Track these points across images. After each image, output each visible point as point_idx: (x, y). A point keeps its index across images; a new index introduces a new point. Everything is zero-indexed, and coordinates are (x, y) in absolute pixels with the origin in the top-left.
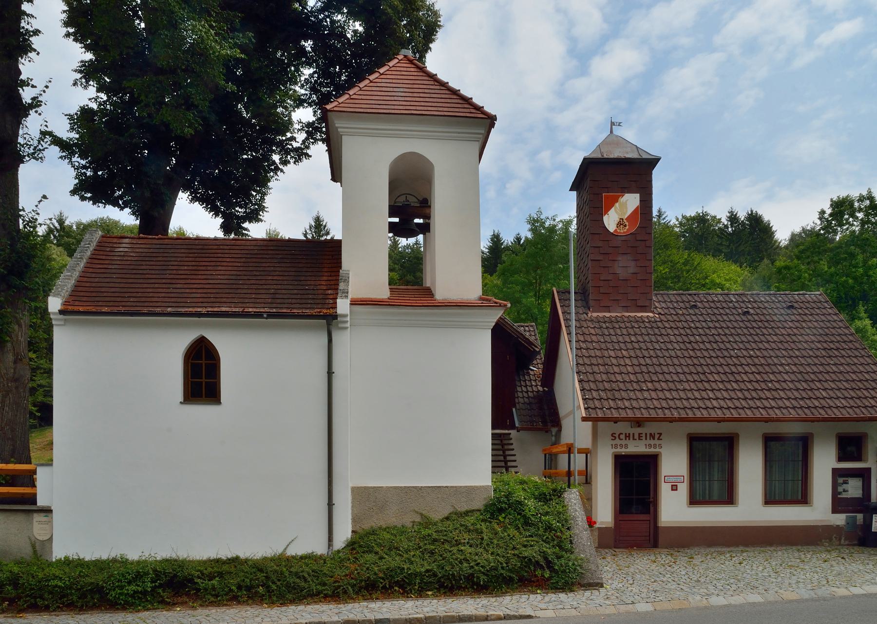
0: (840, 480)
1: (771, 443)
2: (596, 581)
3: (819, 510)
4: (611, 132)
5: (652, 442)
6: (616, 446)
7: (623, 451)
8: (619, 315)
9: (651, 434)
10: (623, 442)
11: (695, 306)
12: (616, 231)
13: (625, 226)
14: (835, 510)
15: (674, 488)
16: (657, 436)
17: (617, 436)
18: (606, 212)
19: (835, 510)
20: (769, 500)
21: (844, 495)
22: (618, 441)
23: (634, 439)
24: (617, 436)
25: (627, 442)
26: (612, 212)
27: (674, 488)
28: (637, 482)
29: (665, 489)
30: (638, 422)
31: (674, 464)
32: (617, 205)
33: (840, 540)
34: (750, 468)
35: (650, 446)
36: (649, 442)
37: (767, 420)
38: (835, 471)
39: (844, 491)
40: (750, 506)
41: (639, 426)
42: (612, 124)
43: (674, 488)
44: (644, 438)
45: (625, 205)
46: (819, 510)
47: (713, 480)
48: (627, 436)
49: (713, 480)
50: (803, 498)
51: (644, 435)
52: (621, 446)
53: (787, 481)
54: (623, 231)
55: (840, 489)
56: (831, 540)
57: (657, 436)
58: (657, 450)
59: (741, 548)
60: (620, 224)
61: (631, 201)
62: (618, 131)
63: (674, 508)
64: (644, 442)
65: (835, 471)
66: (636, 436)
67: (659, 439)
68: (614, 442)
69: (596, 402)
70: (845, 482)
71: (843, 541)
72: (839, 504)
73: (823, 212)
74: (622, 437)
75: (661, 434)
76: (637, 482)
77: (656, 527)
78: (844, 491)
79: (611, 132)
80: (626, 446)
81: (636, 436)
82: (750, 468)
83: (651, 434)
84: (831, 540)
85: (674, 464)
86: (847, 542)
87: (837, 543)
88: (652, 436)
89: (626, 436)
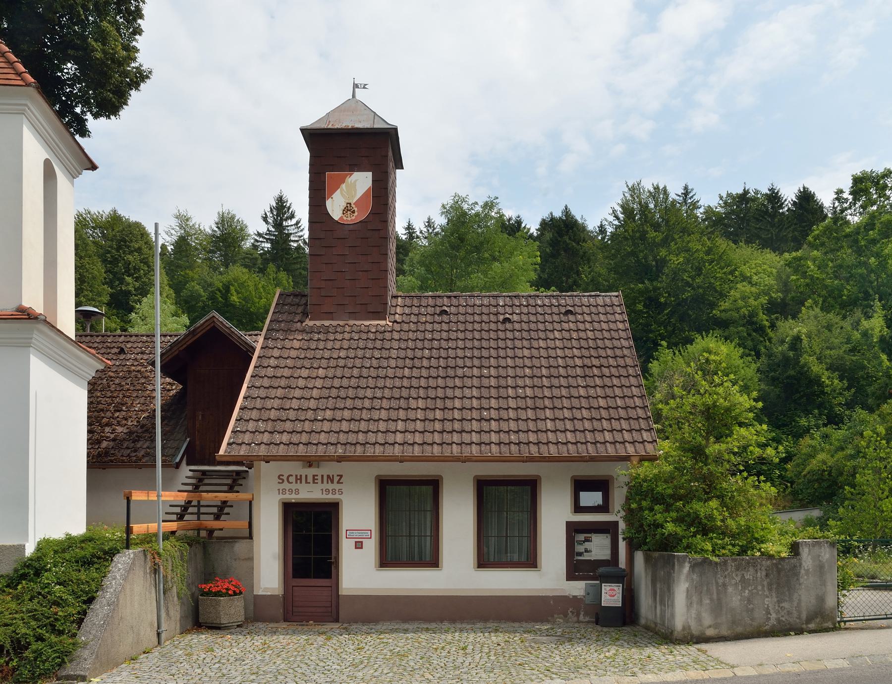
0: (581, 537)
1: (485, 489)
2: (78, 673)
3: (549, 576)
4: (354, 96)
5: (330, 486)
6: (284, 491)
7: (293, 498)
8: (341, 323)
9: (328, 476)
10: (294, 486)
11: (444, 312)
12: (341, 218)
13: (354, 212)
14: (570, 577)
15: (359, 545)
16: (336, 479)
17: (285, 478)
18: (330, 195)
19: (570, 577)
20: (483, 562)
21: (586, 557)
22: (286, 485)
23: (306, 482)
24: (285, 478)
25: (298, 486)
26: (337, 195)
27: (359, 545)
28: (312, 536)
29: (346, 547)
30: (310, 462)
31: (359, 516)
32: (343, 186)
33: (578, 615)
34: (458, 521)
35: (328, 491)
36: (326, 486)
37: (581, 459)
38: (569, 524)
39: (586, 551)
40: (457, 569)
41: (310, 466)
42: (356, 86)
43: (359, 545)
44: (319, 481)
45: (354, 184)
46: (549, 576)
47: (408, 536)
48: (299, 479)
49: (408, 536)
50: (531, 561)
51: (319, 478)
52: (291, 491)
53: (505, 535)
54: (351, 219)
55: (579, 548)
56: (566, 615)
57: (336, 479)
58: (337, 496)
59: (446, 625)
60: (348, 209)
61: (360, 182)
62: (360, 94)
63: (359, 570)
64: (320, 486)
65: (569, 524)
66: (310, 479)
67: (338, 482)
68: (281, 486)
69: (569, 434)
70: (587, 540)
71: (581, 618)
72: (576, 568)
73: (840, 192)
74: (292, 479)
75: (341, 476)
76: (312, 536)
77: (338, 595)
78: (586, 551)
79: (354, 96)
80: (297, 492)
81: (310, 479)
82: (458, 521)
83: (328, 476)
84: (566, 615)
85: (359, 516)
86: (587, 619)
87: (575, 619)
88: (330, 479)
89: (297, 479)
